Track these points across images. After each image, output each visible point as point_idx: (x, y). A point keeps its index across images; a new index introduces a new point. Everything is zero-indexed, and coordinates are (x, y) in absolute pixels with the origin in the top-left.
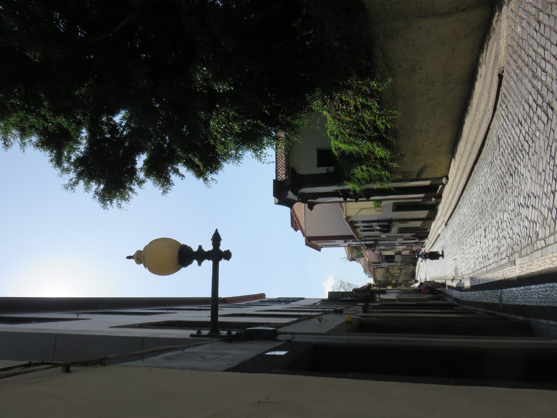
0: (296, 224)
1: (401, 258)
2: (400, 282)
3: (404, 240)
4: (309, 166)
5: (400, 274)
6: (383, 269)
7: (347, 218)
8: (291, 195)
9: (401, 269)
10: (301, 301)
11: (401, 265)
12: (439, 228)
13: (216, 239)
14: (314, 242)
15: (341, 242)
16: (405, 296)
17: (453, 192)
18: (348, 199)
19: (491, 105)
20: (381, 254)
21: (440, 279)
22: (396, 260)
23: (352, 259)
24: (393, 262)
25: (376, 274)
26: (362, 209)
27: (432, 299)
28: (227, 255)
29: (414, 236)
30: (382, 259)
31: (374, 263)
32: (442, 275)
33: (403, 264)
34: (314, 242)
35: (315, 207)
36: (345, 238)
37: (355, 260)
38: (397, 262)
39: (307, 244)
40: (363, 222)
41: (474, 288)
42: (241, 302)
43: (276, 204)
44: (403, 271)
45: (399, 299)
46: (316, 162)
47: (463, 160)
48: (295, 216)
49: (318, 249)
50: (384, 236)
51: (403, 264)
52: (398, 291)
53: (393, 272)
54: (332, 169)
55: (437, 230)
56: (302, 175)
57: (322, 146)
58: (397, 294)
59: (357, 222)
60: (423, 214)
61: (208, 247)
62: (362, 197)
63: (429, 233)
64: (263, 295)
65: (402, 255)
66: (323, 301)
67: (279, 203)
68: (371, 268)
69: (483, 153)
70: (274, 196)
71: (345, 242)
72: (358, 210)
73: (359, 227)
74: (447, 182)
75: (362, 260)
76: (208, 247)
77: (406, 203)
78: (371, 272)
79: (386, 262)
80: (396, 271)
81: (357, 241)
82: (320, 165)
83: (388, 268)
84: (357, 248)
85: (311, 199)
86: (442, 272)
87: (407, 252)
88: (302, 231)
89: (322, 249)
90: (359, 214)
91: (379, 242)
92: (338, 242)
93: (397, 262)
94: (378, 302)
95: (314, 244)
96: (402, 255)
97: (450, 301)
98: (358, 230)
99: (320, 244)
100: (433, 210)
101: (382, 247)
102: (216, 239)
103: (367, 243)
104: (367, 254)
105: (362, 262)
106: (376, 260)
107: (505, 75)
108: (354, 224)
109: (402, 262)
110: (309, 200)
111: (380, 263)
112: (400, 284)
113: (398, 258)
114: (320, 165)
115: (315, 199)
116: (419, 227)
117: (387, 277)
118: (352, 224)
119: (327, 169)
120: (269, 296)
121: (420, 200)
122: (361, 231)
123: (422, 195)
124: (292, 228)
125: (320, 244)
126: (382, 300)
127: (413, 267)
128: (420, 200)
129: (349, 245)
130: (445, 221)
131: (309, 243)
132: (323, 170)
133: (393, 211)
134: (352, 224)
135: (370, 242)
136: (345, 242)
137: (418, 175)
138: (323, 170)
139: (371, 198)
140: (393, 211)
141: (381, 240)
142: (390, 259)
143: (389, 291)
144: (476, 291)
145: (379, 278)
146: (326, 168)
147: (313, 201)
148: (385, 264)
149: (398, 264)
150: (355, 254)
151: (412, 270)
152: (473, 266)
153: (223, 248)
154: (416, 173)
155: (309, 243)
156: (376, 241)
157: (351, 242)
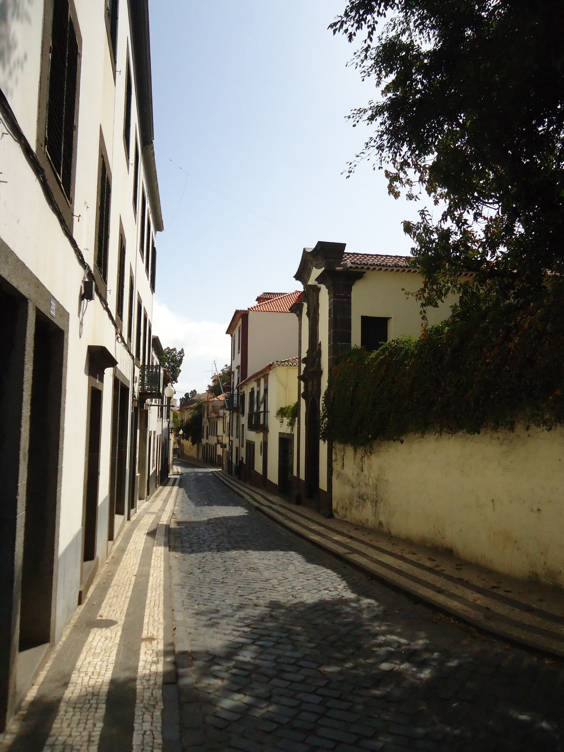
0: (268, 299)
3: (237, 448)
4: (366, 300)
8: (316, 272)
14: (240, 322)
15: (238, 361)
18: (303, 366)
19: (313, 538)
34: (240, 322)
35: (294, 316)
36: (244, 367)
39: (237, 312)
43: (304, 249)
46: (369, 315)
47: (517, 611)
49: (230, 331)
50: (244, 420)
56: (351, 290)
59: (266, 382)
62: (306, 387)
64: (159, 227)
65: (216, 444)
70: (319, 243)
73: (259, 385)
77: (292, 453)
81: (238, 383)
82: (365, 320)
84: (228, 388)
85: (308, 308)
89: (229, 336)
92: (238, 357)
95: (237, 324)
99: (236, 332)
103: (235, 398)
110: (305, 305)
114: (365, 320)
115: (308, 314)
118: (264, 374)
121: (295, 474)
123: (302, 477)
125: (236, 332)
128: (295, 474)
131: (238, 315)
133: (280, 433)
134: (264, 374)
136: (238, 367)
139: (303, 401)
146: (45, 747)
147: (305, 310)
155: (238, 315)
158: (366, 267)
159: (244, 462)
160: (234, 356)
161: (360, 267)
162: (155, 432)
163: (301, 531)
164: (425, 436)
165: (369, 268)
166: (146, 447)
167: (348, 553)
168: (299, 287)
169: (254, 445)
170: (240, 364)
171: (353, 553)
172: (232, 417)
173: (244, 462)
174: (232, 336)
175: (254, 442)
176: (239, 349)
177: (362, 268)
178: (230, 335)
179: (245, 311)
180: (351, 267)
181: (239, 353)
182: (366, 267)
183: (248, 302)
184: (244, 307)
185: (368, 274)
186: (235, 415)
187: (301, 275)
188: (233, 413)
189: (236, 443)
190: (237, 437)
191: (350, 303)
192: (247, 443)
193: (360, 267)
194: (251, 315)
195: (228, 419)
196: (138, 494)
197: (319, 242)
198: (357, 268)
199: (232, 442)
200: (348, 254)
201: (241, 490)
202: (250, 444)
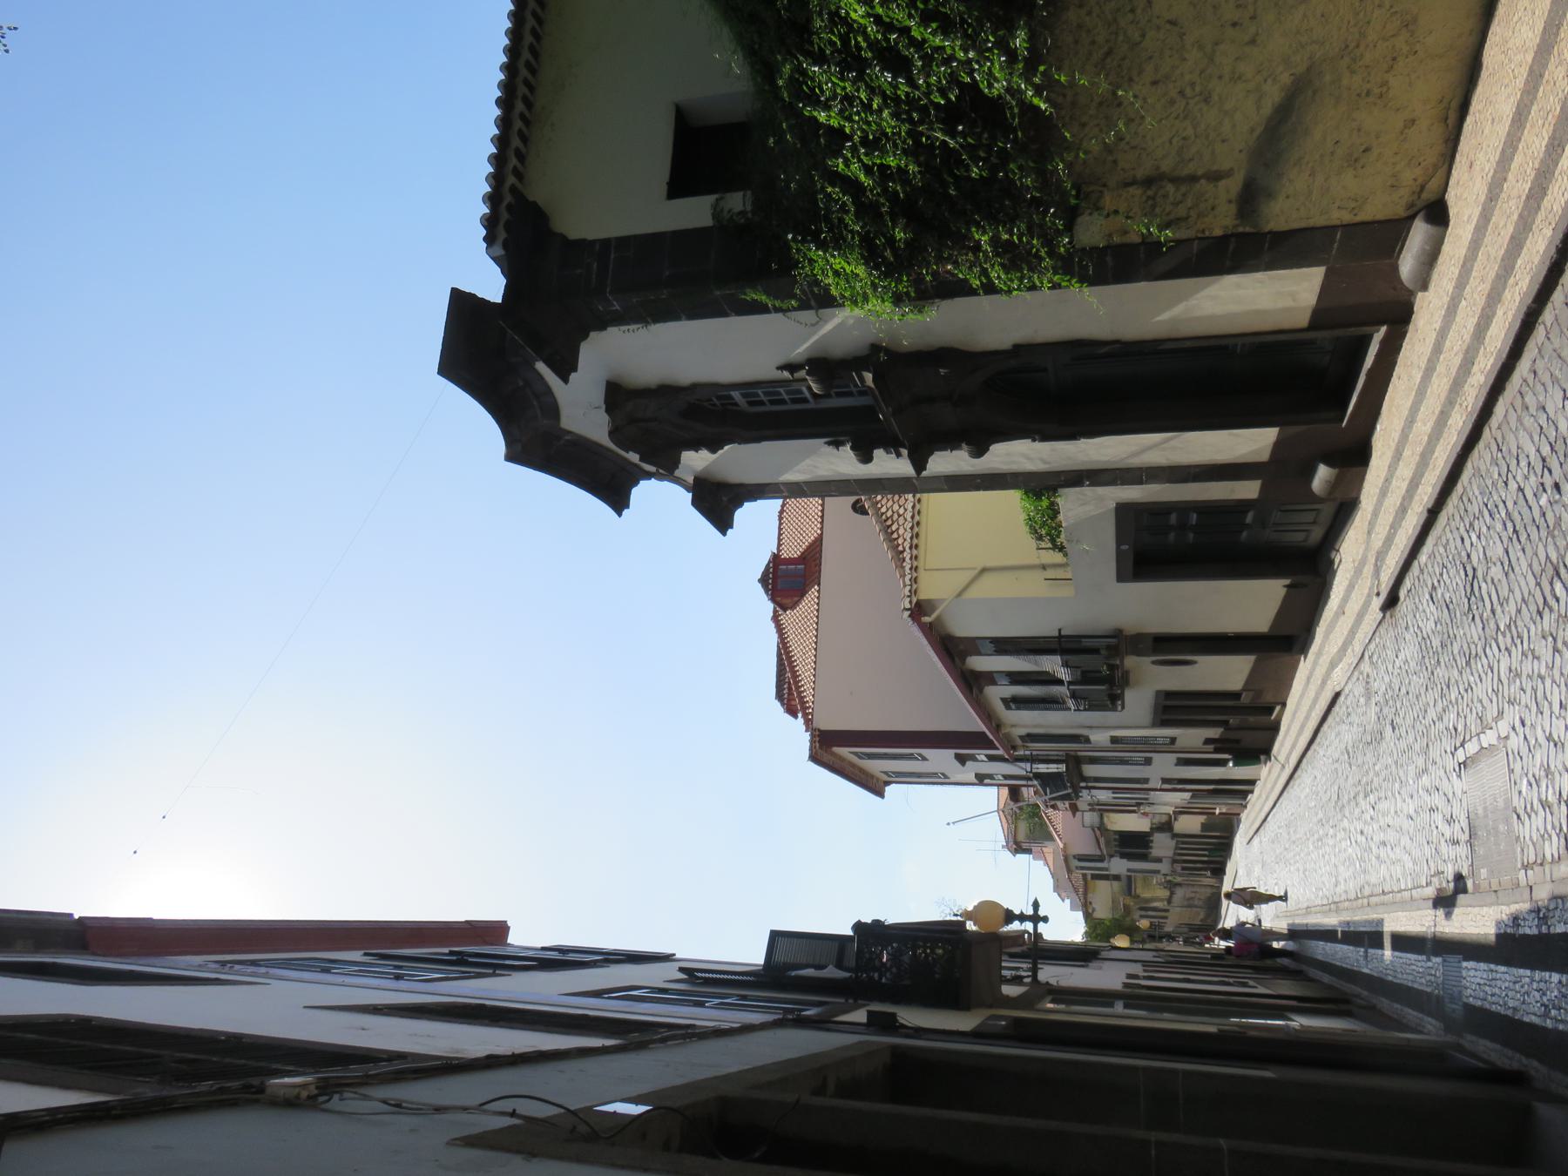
0: (790, 693)
1: (1173, 843)
2: (1168, 929)
5: (1169, 901)
6: (1116, 884)
7: (919, 610)
9: (1171, 886)
11: (1174, 872)
12: (1333, 665)
13: (1036, 905)
14: (844, 752)
15: (941, 758)
16: (1169, 981)
19: (1471, 400)
20: (1102, 828)
21: (1334, 906)
22: (1155, 852)
23: (1017, 847)
24: (1144, 857)
26: (984, 570)
28: (1045, 919)
30: (1107, 843)
31: (1081, 858)
32: (1348, 885)
33: (1178, 867)
36: (960, 742)
37: (1028, 851)
38: (1159, 860)
39: (814, 758)
40: (1004, 646)
41: (1512, 948)
42: (121, 955)
44: (1180, 893)
45: (1132, 997)
46: (664, 189)
48: (792, 668)
49: (876, 787)
51: (1178, 867)
52: (1148, 956)
53: (1146, 895)
54: (737, 202)
56: (583, 244)
58: (1137, 969)
60: (1252, 603)
61: (1030, 912)
63: (1274, 728)
64: (497, 931)
65: (1175, 836)
66: (705, 981)
68: (1079, 876)
69: (1539, 334)
71: (962, 759)
72: (970, 575)
73: (990, 678)
75: (1049, 849)
76: (1030, 912)
78: (1076, 891)
79: (1123, 856)
80: (1155, 892)
82: (678, 187)
83: (1129, 878)
86: (1345, 873)
87: (1190, 824)
88: (805, 715)
90: (967, 595)
91: (1090, 770)
93: (1159, 860)
95: (853, 765)
96: (1175, 836)
97: (1430, 1031)
98: (996, 694)
99: (876, 767)
100: (1309, 571)
101: (1104, 796)
102: (1036, 905)
103: (1042, 768)
104: (1059, 827)
105: (1050, 859)
106: (1089, 848)
107: (1342, 698)
108: (964, 655)
109: (1174, 861)
111: (1101, 859)
112: (1171, 937)
113: (1162, 846)
114: (678, 187)
116: (1235, 695)
117: (1126, 908)
119: (715, 207)
120: (521, 937)
121: (1249, 490)
124: (778, 704)
125: (876, 767)
127: (1209, 881)
128: (1249, 490)
130: (1385, 591)
131: (826, 758)
132: (695, 212)
133: (1121, 578)
135: (1052, 768)
136: (962, 759)
137: (1250, 198)
138: (695, 212)
140: (1121, 578)
141: (1093, 761)
142: (1133, 845)
143: (1114, 954)
145: (1103, 912)
148: (1119, 866)
149: (1164, 867)
150: (1025, 834)
151: (1209, 891)
153: (1041, 913)
154: (1233, 185)
155: (826, 758)
156: (1074, 762)
159: (1214, 733)
160: (934, 775)
162: (1130, 976)
163: (1401, 547)
169: (1169, 695)
170: (951, 752)
172: (1097, 780)
173: (1214, 733)
174: (888, 783)
175: (1158, 693)
176: (910, 757)
178: (887, 788)
179: (812, 736)
181: (924, 759)
183: (797, 735)
185: (538, 192)
186: (1090, 770)
188: (1085, 779)
190: (1148, 762)
191: (623, 242)
192: (1164, 723)
195: (1104, 796)
196: (1299, 1022)
197: (511, 457)
199: (1165, 781)
202: (1166, 709)
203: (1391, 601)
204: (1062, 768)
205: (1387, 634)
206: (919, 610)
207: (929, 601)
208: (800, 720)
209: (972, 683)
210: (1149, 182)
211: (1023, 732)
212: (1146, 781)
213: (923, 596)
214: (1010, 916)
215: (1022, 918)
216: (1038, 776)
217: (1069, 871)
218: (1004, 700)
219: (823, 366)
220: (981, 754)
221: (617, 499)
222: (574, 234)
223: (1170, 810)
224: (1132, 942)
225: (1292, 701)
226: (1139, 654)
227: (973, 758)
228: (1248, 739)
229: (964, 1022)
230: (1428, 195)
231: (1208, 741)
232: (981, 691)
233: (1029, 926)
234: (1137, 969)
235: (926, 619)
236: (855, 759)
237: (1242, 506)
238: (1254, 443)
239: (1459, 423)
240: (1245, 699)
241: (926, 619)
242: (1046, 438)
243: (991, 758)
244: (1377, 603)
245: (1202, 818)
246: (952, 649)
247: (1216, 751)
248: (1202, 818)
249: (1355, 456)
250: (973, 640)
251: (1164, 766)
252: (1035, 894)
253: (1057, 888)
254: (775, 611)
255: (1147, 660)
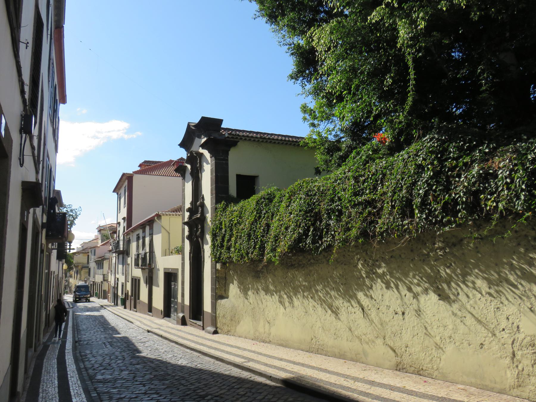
7: (159, 216)
10: (54, 145)
12: (140, 322)
15: (124, 213)
16: (53, 283)
17: (200, 341)
25: (81, 255)
26: (169, 233)
27: (48, 316)
29: (127, 295)
33: (92, 283)
36: (129, 219)
38: (94, 277)
39: (124, 175)
45: (49, 274)
49: (117, 190)
51: (92, 283)
52: (60, 275)
55: (137, 320)
56: (228, 154)
57: (261, 181)
58: (56, 273)
60: (159, 303)
61: (72, 247)
64: (64, 100)
67: (189, 125)
68: (87, 250)
70: (203, 118)
71: (124, 219)
72: (168, 230)
73: (144, 232)
74: (209, 333)
76: (72, 247)
78: (83, 250)
81: (124, 231)
82: (239, 177)
83: (88, 267)
89: (115, 194)
90: (162, 229)
94: (47, 245)
95: (123, 185)
96: (102, 282)
98: (140, 232)
100: (167, 313)
103: (121, 243)
108: (149, 225)
109: (94, 282)
114: (239, 177)
116: (139, 299)
120: (62, 108)
121: (180, 300)
122: (138, 235)
124: (143, 161)
125: (122, 191)
126: (50, 252)
129: (119, 223)
130: (152, 330)
131: (124, 178)
133: (165, 269)
136: (124, 219)
140: (165, 269)
141: (123, 258)
143: (61, 265)
144: (59, 387)
145: (76, 260)
150: (107, 233)
152: (99, 377)
157: (123, 224)
158: (239, 138)
159: (130, 294)
160: (120, 210)
161: (235, 137)
162: (54, 272)
164: (166, 318)
165: (241, 139)
166: (38, 93)
167: (245, 362)
168: (183, 154)
169: (139, 280)
170: (126, 216)
171: (249, 361)
173: (130, 294)
176: (125, 204)
177: (237, 138)
179: (131, 174)
180: (228, 137)
182: (239, 138)
183: (132, 167)
184: (130, 171)
187: (186, 144)
189: (122, 279)
190: (123, 274)
191: (227, 164)
192: (132, 279)
193: (235, 137)
194: (136, 178)
198: (232, 138)
199: (118, 279)
200: (223, 129)
201: (223, 351)
202: (136, 280)
203: (149, 331)
204: (121, 249)
205: (141, 331)
206: (159, 216)
207: (161, 218)
208: (139, 169)
209: (142, 226)
210: (225, 278)
211: (131, 238)
212: (118, 273)
213: (162, 217)
214: (70, 242)
215: (70, 246)
216: (118, 242)
217: (90, 248)
218: (139, 234)
219: (203, 205)
220: (125, 225)
221: (182, 145)
222: (230, 152)
223: (109, 280)
224: (65, 270)
225: (137, 314)
226: (149, 273)
227: (124, 222)
228: (128, 303)
229: (44, 241)
230: (219, 331)
231: (128, 291)
232: (141, 228)
233: (68, 247)
234: (56, 273)
235: (156, 218)
236: (124, 186)
237: (177, 299)
238: (187, 302)
239: (193, 345)
240: (138, 301)
241: (156, 218)
242: (190, 253)
243: (124, 227)
244: (149, 329)
245: (107, 290)
246: (150, 222)
247: (125, 294)
248: (107, 290)
249: (184, 322)
250: (152, 228)
251: (122, 279)
252: (82, 234)
253: (85, 243)
254: (173, 161)
255: (147, 275)
